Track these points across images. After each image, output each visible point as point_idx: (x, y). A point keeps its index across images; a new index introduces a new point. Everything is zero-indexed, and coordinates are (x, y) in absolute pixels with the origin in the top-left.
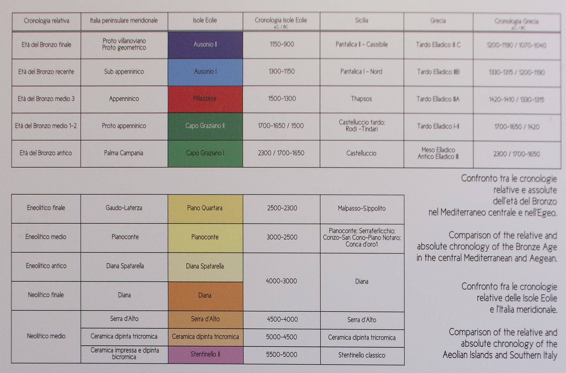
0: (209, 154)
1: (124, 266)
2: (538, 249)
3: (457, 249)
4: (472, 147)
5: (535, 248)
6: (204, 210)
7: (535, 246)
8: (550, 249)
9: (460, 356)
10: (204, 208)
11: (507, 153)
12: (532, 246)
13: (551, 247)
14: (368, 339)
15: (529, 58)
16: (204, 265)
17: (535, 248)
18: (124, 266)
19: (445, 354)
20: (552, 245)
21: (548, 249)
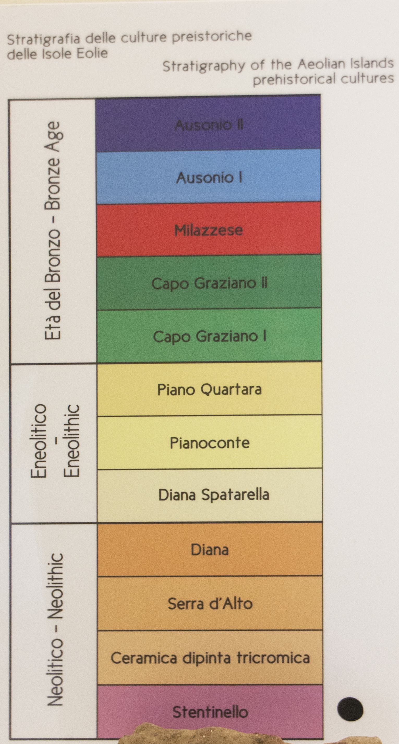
0: (201, 233)
1: (210, 495)
2: (56, 162)
3: (61, 567)
4: (232, 629)
5: (55, 168)
6: (207, 394)
7: (50, 169)
8: (56, 136)
9: (193, 232)
10: (207, 389)
11: (243, 607)
12: (49, 176)
13: (52, 135)
14: (228, 660)
15: (294, 360)
16: (212, 493)
17: (55, 168)
18: (210, 495)
19: (228, 602)
20: (47, 134)
21: (56, 140)
